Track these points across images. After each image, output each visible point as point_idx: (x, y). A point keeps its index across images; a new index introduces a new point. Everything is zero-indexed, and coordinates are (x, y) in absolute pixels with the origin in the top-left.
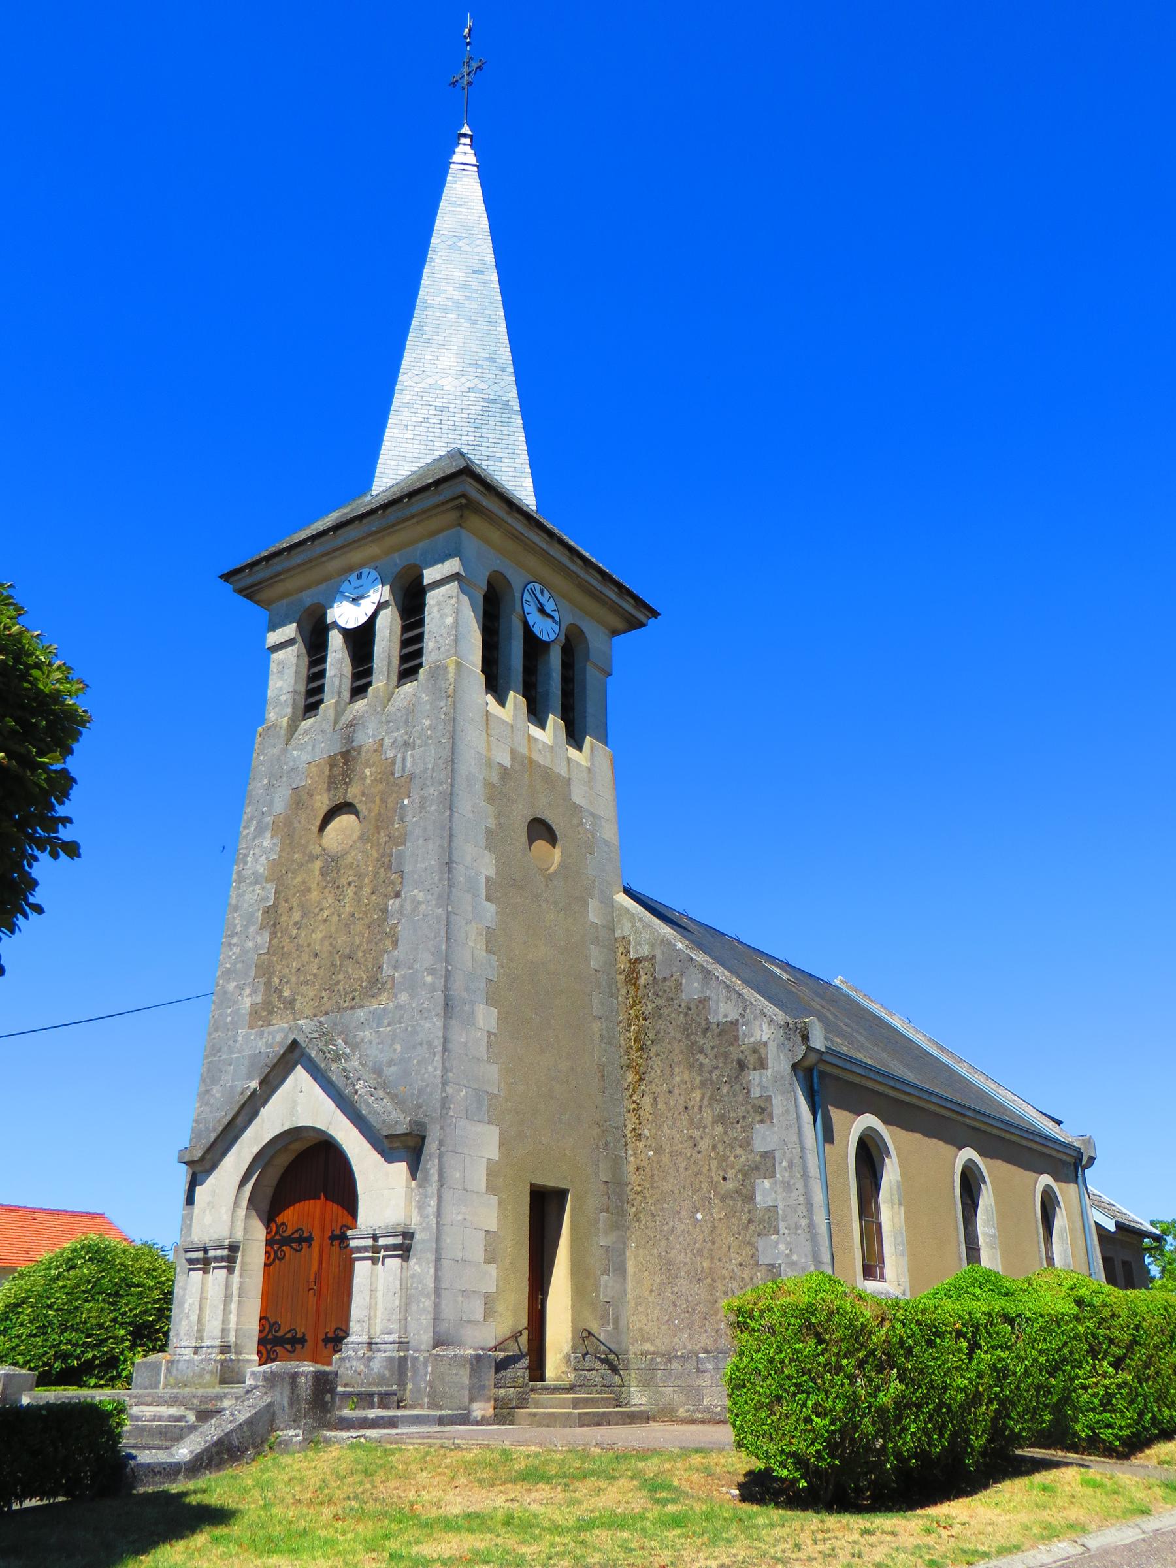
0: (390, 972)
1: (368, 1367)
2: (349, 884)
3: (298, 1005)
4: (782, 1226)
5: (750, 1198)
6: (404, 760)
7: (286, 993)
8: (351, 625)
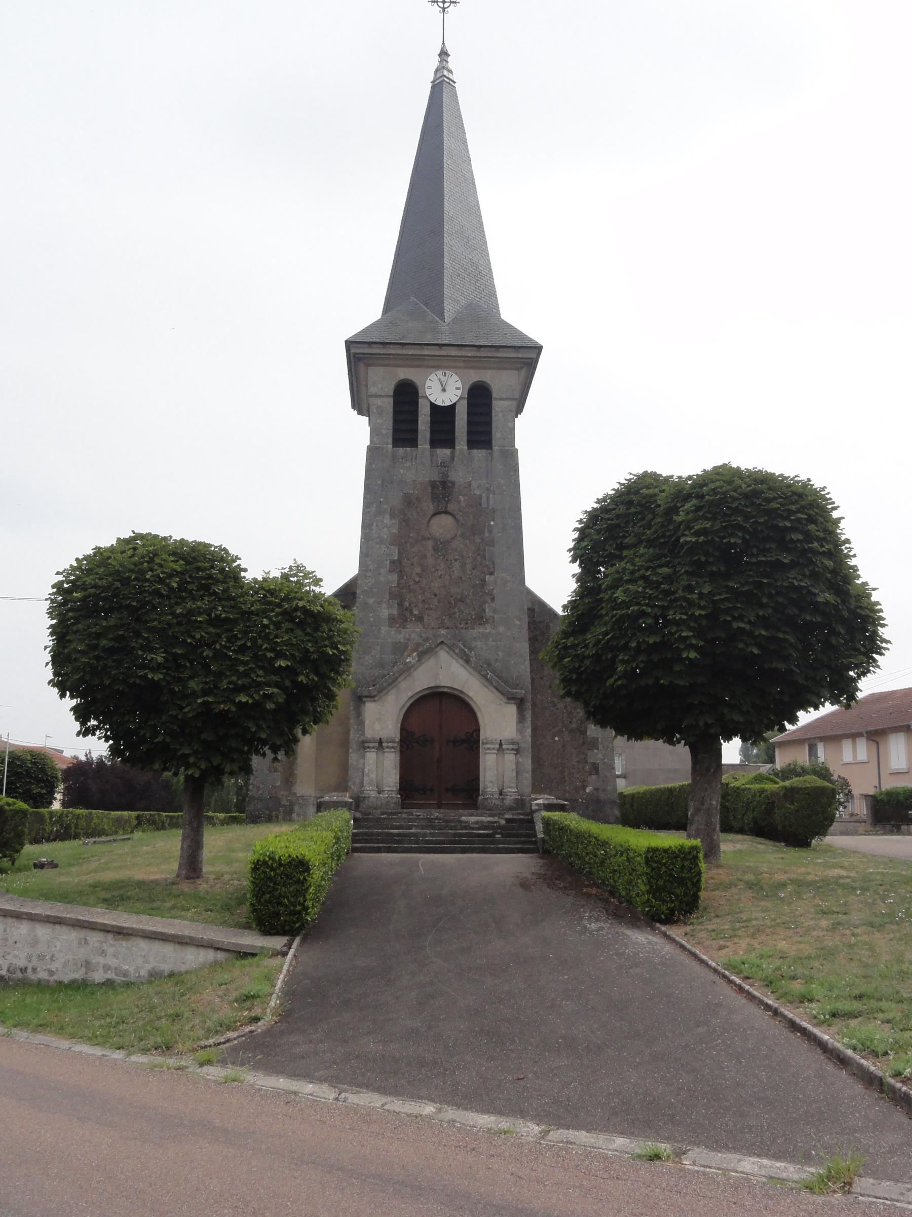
0: (491, 614)
1: (503, 802)
2: (456, 560)
3: (426, 620)
4: (600, 747)
5: (584, 732)
6: (488, 500)
7: (416, 612)
8: (439, 403)
